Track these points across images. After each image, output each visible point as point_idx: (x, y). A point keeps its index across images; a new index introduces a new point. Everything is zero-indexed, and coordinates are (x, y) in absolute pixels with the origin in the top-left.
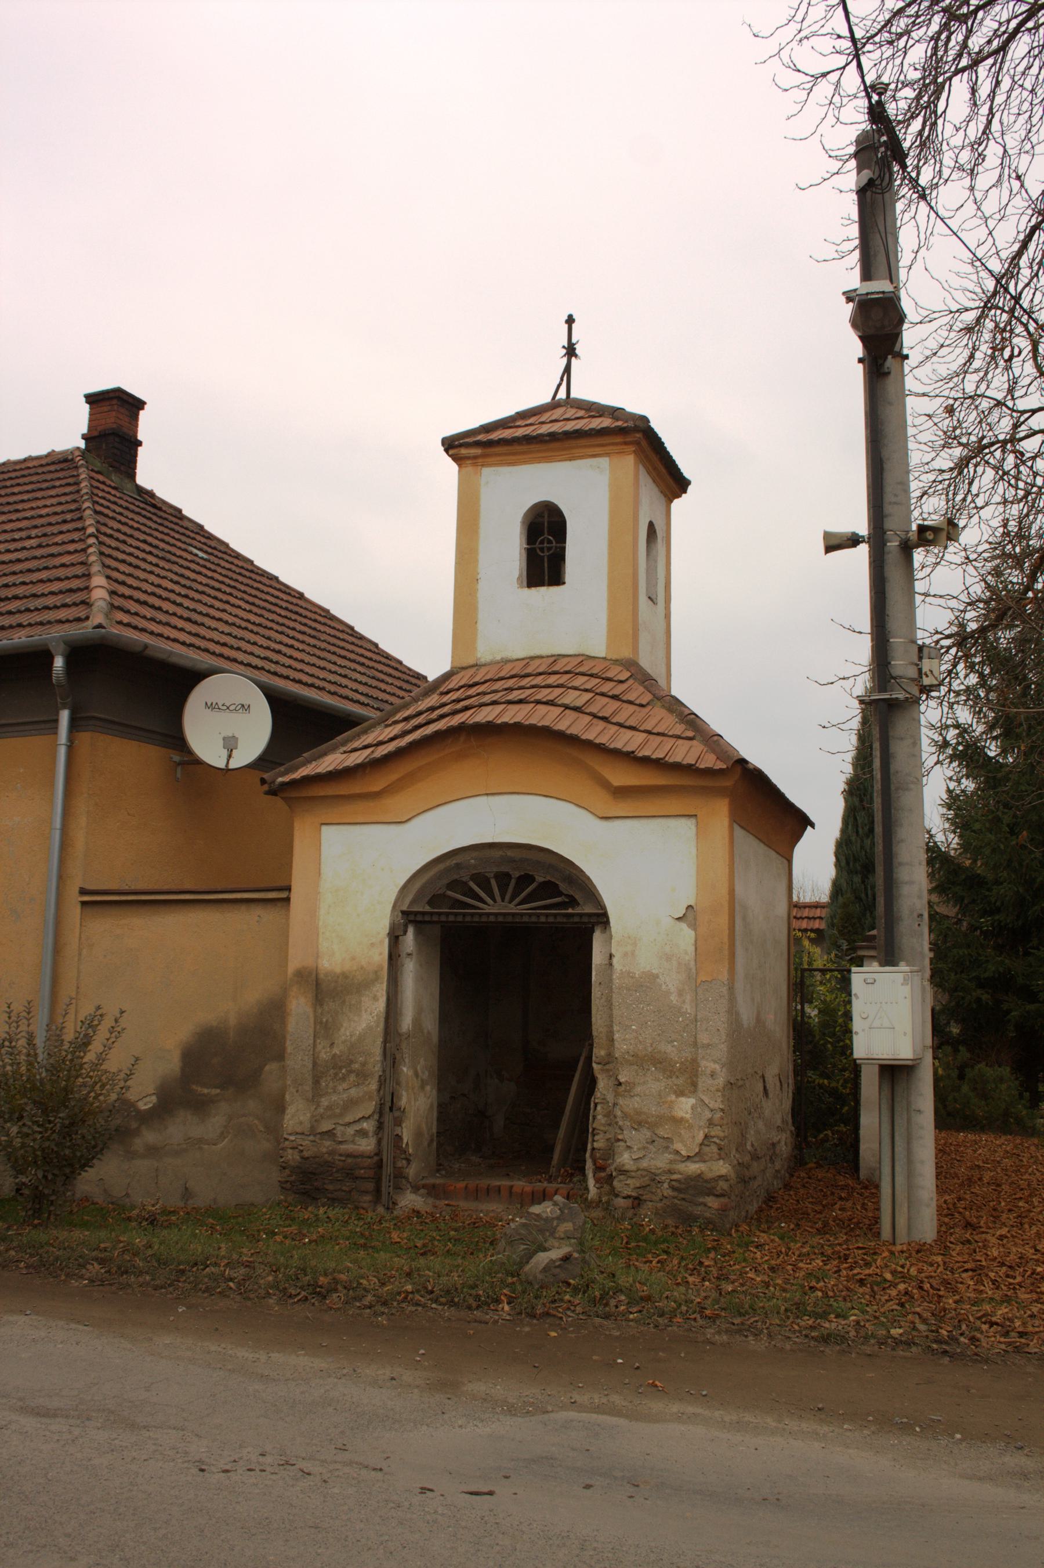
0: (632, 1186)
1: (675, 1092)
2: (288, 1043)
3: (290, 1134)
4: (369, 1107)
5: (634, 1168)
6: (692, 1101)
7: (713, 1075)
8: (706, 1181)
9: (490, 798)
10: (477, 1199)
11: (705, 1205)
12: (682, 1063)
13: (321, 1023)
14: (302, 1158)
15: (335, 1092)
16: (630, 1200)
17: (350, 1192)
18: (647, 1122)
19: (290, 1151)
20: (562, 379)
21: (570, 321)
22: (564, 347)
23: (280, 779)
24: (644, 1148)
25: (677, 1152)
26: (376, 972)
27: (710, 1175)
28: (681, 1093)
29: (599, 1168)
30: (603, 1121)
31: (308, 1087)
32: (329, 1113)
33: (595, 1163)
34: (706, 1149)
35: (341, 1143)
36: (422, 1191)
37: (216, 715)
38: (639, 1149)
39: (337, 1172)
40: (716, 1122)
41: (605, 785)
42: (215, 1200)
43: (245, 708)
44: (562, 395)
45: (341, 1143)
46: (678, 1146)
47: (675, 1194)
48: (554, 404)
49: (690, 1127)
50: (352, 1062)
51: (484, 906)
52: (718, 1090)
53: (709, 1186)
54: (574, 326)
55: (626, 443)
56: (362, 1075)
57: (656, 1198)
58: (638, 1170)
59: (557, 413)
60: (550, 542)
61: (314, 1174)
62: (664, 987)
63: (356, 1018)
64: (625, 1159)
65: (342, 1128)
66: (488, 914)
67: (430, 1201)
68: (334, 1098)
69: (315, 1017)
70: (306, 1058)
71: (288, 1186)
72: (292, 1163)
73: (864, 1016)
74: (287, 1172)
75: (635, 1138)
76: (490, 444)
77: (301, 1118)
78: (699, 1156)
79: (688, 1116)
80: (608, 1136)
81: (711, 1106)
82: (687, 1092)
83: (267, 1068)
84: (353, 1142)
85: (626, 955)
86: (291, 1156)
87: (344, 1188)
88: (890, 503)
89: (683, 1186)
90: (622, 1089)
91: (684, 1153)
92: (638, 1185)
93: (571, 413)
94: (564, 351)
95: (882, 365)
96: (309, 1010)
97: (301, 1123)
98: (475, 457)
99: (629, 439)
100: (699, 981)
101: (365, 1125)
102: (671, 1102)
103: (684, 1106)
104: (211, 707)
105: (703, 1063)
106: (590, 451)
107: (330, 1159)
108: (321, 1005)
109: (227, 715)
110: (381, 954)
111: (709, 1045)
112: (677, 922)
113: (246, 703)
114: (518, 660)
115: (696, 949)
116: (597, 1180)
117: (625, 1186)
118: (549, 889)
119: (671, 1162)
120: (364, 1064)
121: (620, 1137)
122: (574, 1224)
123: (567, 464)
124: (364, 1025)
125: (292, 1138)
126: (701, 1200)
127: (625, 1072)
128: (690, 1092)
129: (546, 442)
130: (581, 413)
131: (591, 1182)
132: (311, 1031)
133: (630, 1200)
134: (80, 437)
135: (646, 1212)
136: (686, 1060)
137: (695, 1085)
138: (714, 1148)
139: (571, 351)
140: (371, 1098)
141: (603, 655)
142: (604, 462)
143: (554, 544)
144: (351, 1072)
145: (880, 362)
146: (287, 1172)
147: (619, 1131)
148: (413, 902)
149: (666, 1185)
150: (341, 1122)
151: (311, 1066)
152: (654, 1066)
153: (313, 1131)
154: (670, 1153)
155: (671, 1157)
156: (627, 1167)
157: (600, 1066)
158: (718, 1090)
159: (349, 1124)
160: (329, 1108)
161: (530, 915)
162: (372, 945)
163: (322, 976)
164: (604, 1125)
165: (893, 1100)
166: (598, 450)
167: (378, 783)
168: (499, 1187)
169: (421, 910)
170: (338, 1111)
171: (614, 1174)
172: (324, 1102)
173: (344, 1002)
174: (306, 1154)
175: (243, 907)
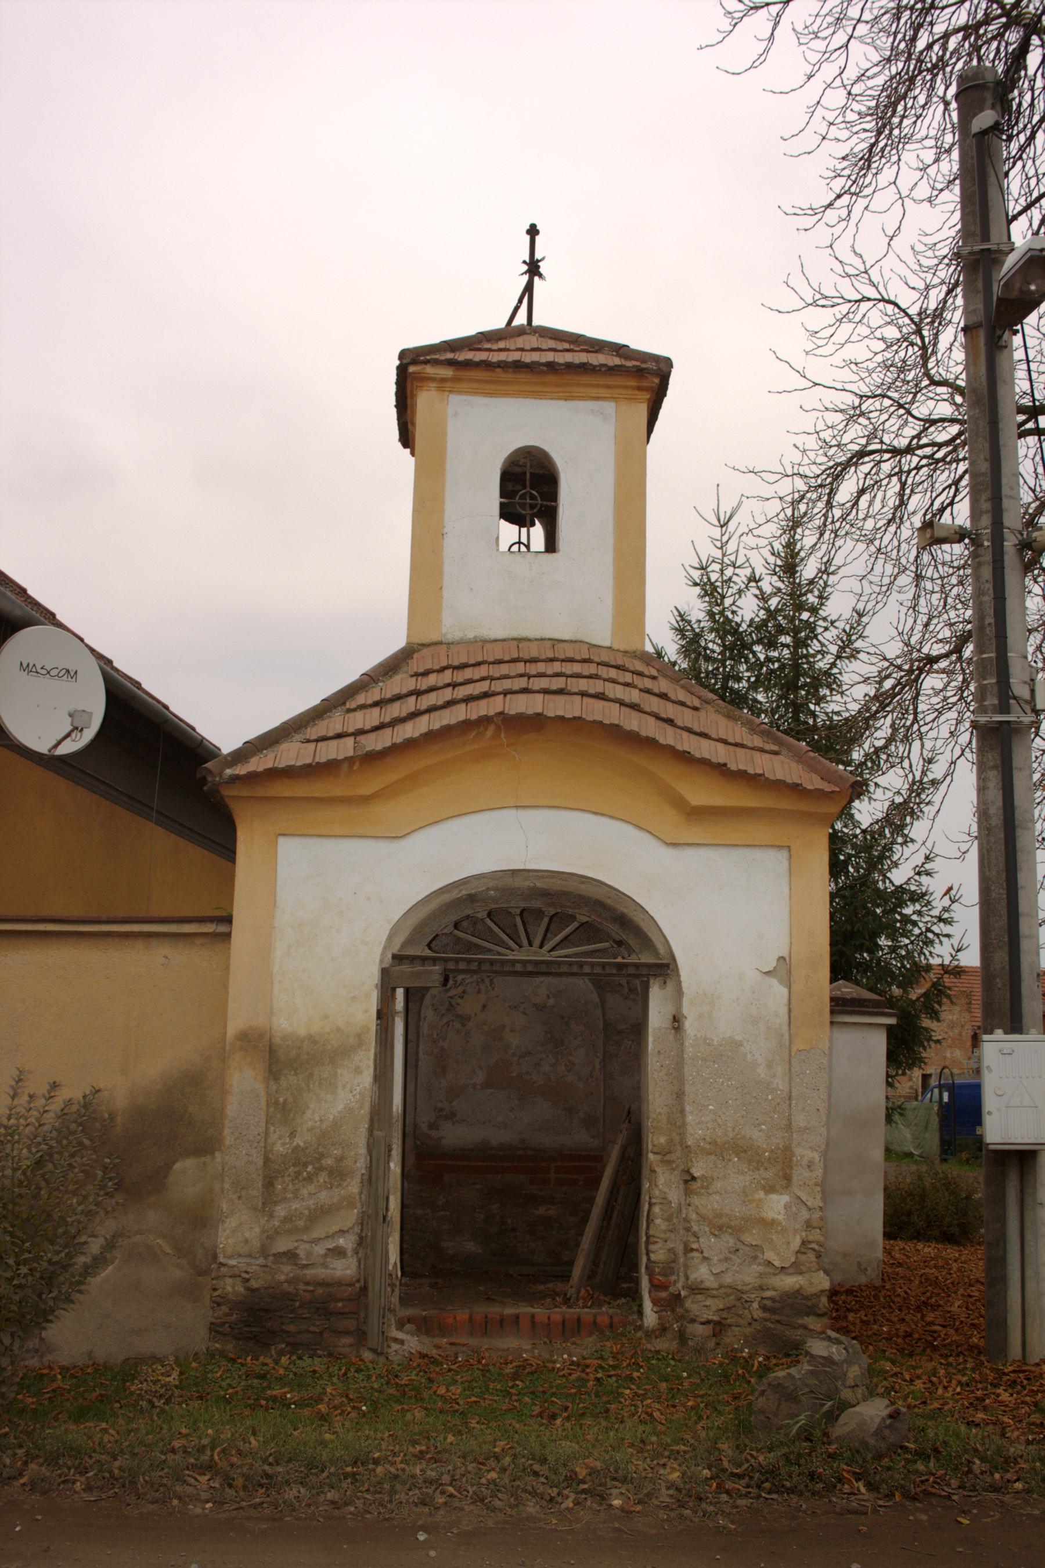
0: (714, 1308)
1: (764, 1188)
2: (227, 1132)
3: (230, 1257)
4: (350, 1217)
5: (715, 1285)
6: (785, 1198)
7: (810, 1165)
8: (806, 1298)
9: (521, 812)
10: (485, 1334)
11: (805, 1327)
12: (772, 1151)
13: (276, 1103)
14: (248, 1289)
15: (296, 1197)
16: (711, 1326)
17: (321, 1333)
18: (730, 1227)
19: (229, 1281)
20: (520, 301)
21: (533, 231)
22: (524, 262)
23: (229, 771)
24: (726, 1259)
25: (769, 1263)
26: (359, 1036)
27: (811, 1290)
28: (770, 1189)
29: (655, 1286)
30: (663, 1227)
31: (256, 1191)
32: (288, 1226)
33: (651, 1281)
34: (803, 1258)
35: (305, 1266)
36: (408, 1326)
37: (32, 679)
38: (720, 1261)
39: (302, 1306)
40: (815, 1224)
41: (679, 804)
42: (90, 1354)
43: (70, 674)
44: (521, 319)
45: (305, 1266)
46: (769, 1255)
47: (767, 1315)
48: (509, 332)
49: (784, 1230)
50: (322, 1156)
51: (508, 952)
52: (816, 1185)
53: (810, 1303)
54: (537, 238)
55: (639, 388)
56: (338, 1174)
57: (744, 1322)
58: (721, 1286)
59: (520, 342)
60: (532, 497)
61: (267, 1311)
62: (749, 1057)
63: (329, 1097)
64: (702, 1273)
65: (307, 1246)
66: (513, 962)
67: (426, 1340)
68: (295, 1205)
69: (268, 1095)
70: (254, 1152)
71: (226, 1329)
72: (231, 1297)
73: (1000, 1093)
74: (225, 1309)
75: (713, 1245)
76: (468, 364)
77: (247, 1235)
78: (796, 1268)
79: (780, 1217)
80: (670, 1245)
81: (809, 1204)
82: (778, 1187)
83: (178, 1166)
84: (325, 1266)
85: (701, 1016)
86: (231, 1287)
87: (312, 1329)
88: (1006, 496)
89: (777, 1305)
90: (695, 1186)
91: (777, 1263)
92: (721, 1307)
93: (533, 341)
94: (525, 268)
95: (1000, 337)
96: (260, 1086)
97: (246, 1241)
98: (443, 380)
99: (645, 384)
100: (794, 1050)
101: (341, 1241)
102: (760, 1200)
103: (776, 1205)
104: (28, 668)
105: (798, 1151)
106: (594, 392)
107: (291, 1289)
108: (276, 1079)
109: (46, 681)
110: (366, 1011)
111: (806, 1128)
112: (767, 978)
113: (72, 668)
114: (496, 641)
115: (790, 1011)
116: (655, 1302)
117: (703, 1308)
118: (588, 932)
119: (761, 1275)
120: (340, 1159)
121: (695, 1246)
122: (860, 1365)
123: (562, 403)
124: (341, 1107)
125: (232, 1262)
126: (800, 1321)
127: (701, 1164)
128: (782, 1187)
129: (542, 373)
130: (566, 346)
131: (648, 1306)
132: (262, 1115)
133: (711, 1326)
134: (541, 231)
135: (733, 1338)
136: (778, 1148)
137: (788, 1178)
138: (812, 1256)
139: (533, 268)
140: (351, 1205)
141: (607, 644)
142: (609, 407)
143: (539, 502)
144: (321, 1169)
145: (998, 332)
146: (225, 1309)
147: (692, 1239)
148: (406, 944)
149: (755, 1305)
150: (305, 1238)
151: (260, 1162)
152: (737, 1155)
153: (264, 1251)
154: (760, 1264)
155: (761, 1268)
156: (707, 1284)
157: (658, 1157)
158: (816, 1185)
159: (316, 1241)
160: (288, 1219)
161: (571, 964)
162: (354, 999)
163: (277, 1040)
164: (665, 1232)
165: (1022, 1191)
166: (602, 392)
167: (373, 783)
168: (517, 1316)
169: (419, 954)
170: (301, 1223)
171: (683, 1293)
172: (281, 1211)
173: (311, 1075)
174: (254, 1284)
175: (140, 944)
